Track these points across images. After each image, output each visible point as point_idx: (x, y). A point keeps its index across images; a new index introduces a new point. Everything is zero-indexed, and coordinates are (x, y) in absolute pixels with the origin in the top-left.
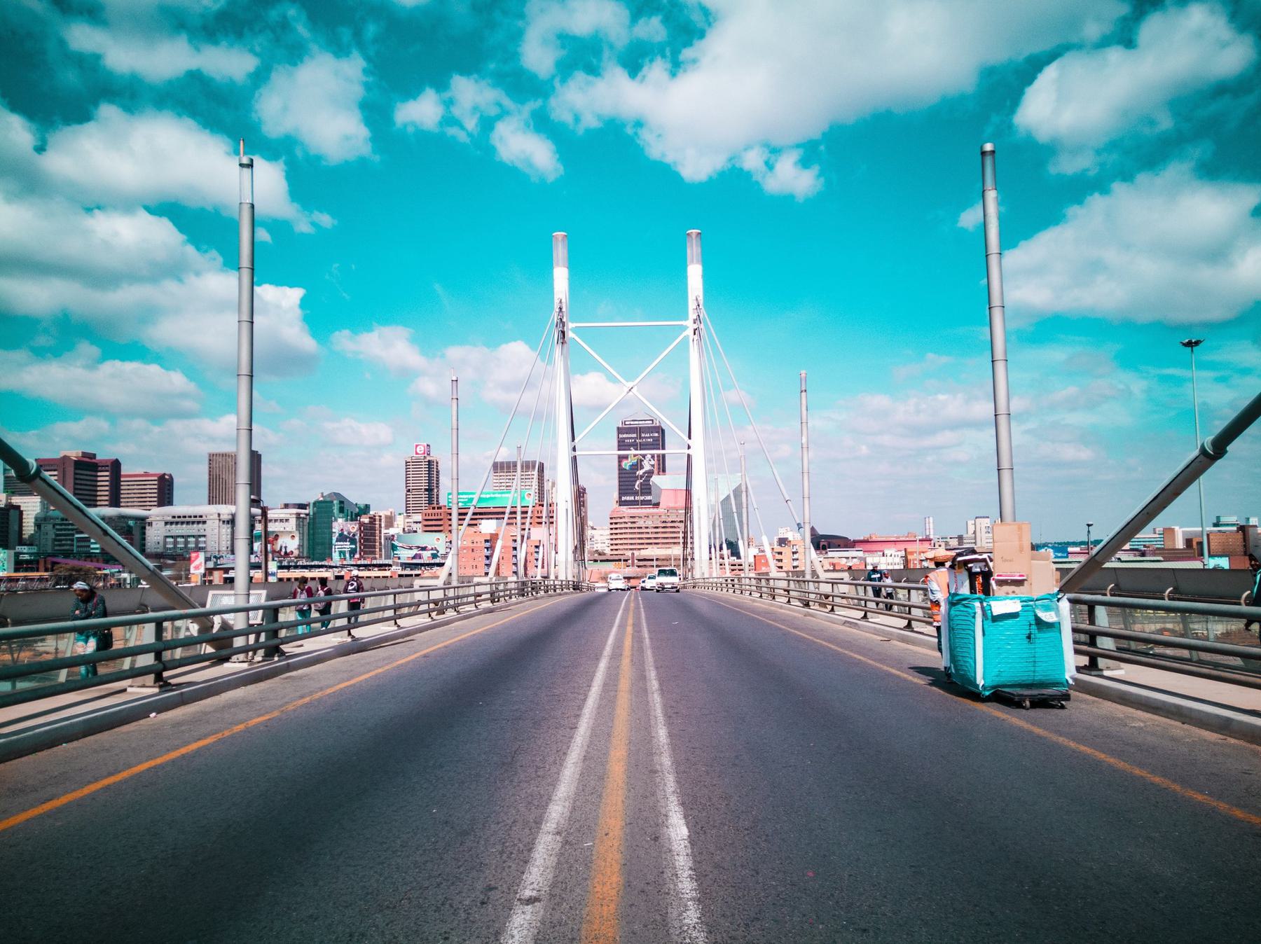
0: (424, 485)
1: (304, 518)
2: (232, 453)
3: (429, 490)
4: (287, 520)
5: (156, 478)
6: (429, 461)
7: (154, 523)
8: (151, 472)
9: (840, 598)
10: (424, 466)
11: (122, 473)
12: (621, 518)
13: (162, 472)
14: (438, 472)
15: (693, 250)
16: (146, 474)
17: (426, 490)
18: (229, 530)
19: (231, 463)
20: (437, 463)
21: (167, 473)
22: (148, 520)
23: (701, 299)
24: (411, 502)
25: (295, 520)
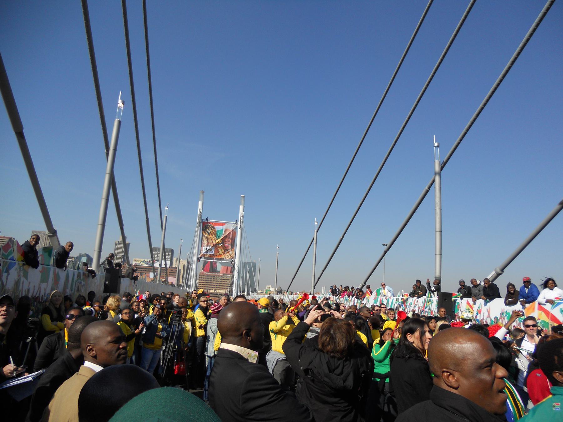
8: (6, 236)
17: (122, 256)
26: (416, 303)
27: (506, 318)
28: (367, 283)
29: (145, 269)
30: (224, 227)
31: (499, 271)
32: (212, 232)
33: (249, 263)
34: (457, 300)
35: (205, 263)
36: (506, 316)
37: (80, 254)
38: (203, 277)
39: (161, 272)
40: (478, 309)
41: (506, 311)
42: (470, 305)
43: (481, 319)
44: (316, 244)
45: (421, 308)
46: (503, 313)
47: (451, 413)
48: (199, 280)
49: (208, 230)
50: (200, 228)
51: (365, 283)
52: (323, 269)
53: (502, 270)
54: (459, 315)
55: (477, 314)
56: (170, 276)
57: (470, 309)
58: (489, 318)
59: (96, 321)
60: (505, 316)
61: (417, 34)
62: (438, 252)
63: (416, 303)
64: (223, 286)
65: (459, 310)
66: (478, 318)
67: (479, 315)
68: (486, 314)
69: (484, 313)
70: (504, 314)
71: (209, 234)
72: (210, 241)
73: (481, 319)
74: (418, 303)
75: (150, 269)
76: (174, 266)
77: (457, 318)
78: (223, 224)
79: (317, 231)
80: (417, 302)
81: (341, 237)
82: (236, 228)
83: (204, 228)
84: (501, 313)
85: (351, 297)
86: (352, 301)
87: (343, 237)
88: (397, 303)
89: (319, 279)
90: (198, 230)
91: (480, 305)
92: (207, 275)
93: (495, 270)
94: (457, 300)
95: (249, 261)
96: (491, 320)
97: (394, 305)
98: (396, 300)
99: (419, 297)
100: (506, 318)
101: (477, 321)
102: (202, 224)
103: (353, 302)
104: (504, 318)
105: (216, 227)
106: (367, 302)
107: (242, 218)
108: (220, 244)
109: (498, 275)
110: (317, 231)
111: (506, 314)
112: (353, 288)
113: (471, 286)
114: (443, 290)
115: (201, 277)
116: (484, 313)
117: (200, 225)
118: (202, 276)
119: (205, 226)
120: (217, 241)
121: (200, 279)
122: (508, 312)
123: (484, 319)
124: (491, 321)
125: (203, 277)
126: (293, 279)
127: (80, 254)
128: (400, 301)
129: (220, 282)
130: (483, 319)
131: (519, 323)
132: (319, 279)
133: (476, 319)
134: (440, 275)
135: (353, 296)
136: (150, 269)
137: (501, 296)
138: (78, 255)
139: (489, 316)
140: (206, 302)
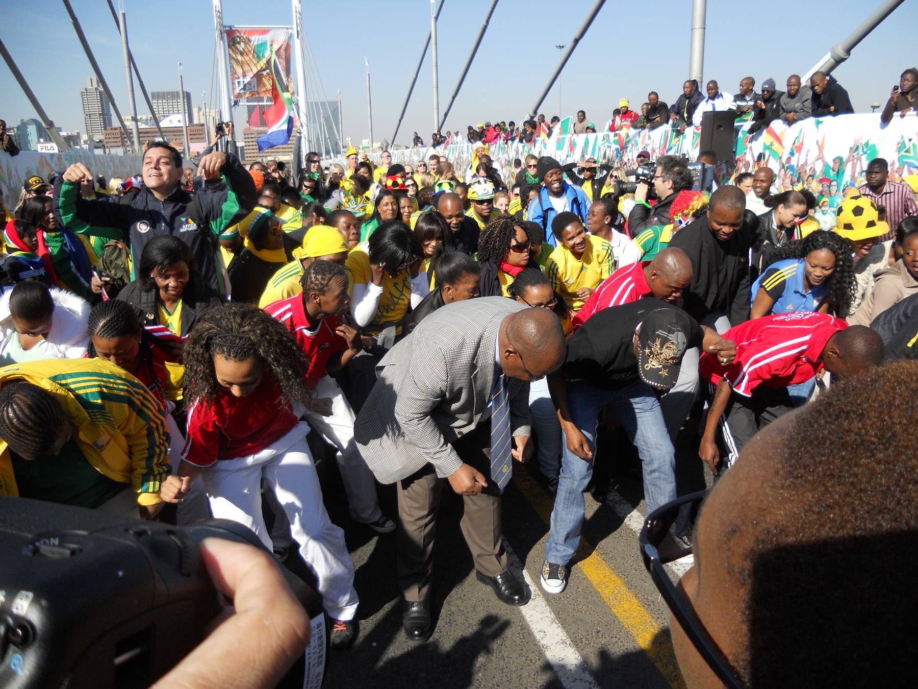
17: (100, 115)
26: (647, 141)
27: (864, 157)
28: (539, 112)
29: (146, 133)
30: (267, 38)
31: (841, 52)
32: (246, 50)
33: (323, 104)
34: (742, 126)
35: (250, 110)
36: (865, 153)
37: (22, 121)
38: (250, 136)
39: (139, 138)
40: (794, 143)
41: (867, 143)
42: (776, 135)
43: (799, 165)
44: (436, 44)
45: (657, 151)
46: (857, 148)
49: (237, 45)
50: (224, 44)
51: (535, 112)
52: (452, 94)
53: (848, 51)
54: (747, 160)
55: (792, 154)
56: (192, 141)
57: (776, 144)
58: (820, 160)
60: (862, 153)
62: (698, 23)
63: (647, 141)
65: (746, 148)
66: (794, 162)
67: (796, 155)
68: (815, 152)
69: (808, 151)
70: (861, 149)
71: (242, 54)
72: (246, 68)
73: (799, 165)
74: (651, 141)
75: (155, 132)
76: (196, 122)
77: (741, 165)
78: (265, 32)
79: (436, 18)
80: (650, 138)
81: (484, 23)
82: (291, 36)
83: (231, 43)
84: (851, 148)
85: (510, 142)
86: (514, 149)
87: (488, 22)
88: (606, 145)
89: (446, 115)
90: (221, 48)
91: (800, 132)
92: (256, 131)
93: (832, 50)
94: (742, 126)
95: (323, 99)
96: (825, 165)
97: (600, 149)
98: (604, 139)
99: (653, 128)
100: (864, 157)
101: (791, 170)
102: (225, 34)
103: (514, 153)
104: (859, 159)
105: (252, 38)
106: (543, 149)
107: (298, 15)
108: (264, 70)
109: (839, 61)
110: (436, 18)
111: (865, 150)
112: (512, 124)
113: (784, 89)
114: (638, 109)
115: (247, 136)
116: (808, 151)
117: (222, 38)
119: (231, 37)
120: (259, 68)
121: (247, 140)
122: (870, 143)
123: (809, 163)
124: (824, 166)
125: (250, 136)
126: (400, 121)
127: (22, 121)
128: (611, 141)
130: (806, 163)
131: (898, 168)
132: (446, 115)
133: (787, 165)
134: (700, 76)
135: (513, 139)
136: (155, 132)
138: (19, 123)
139: (820, 157)
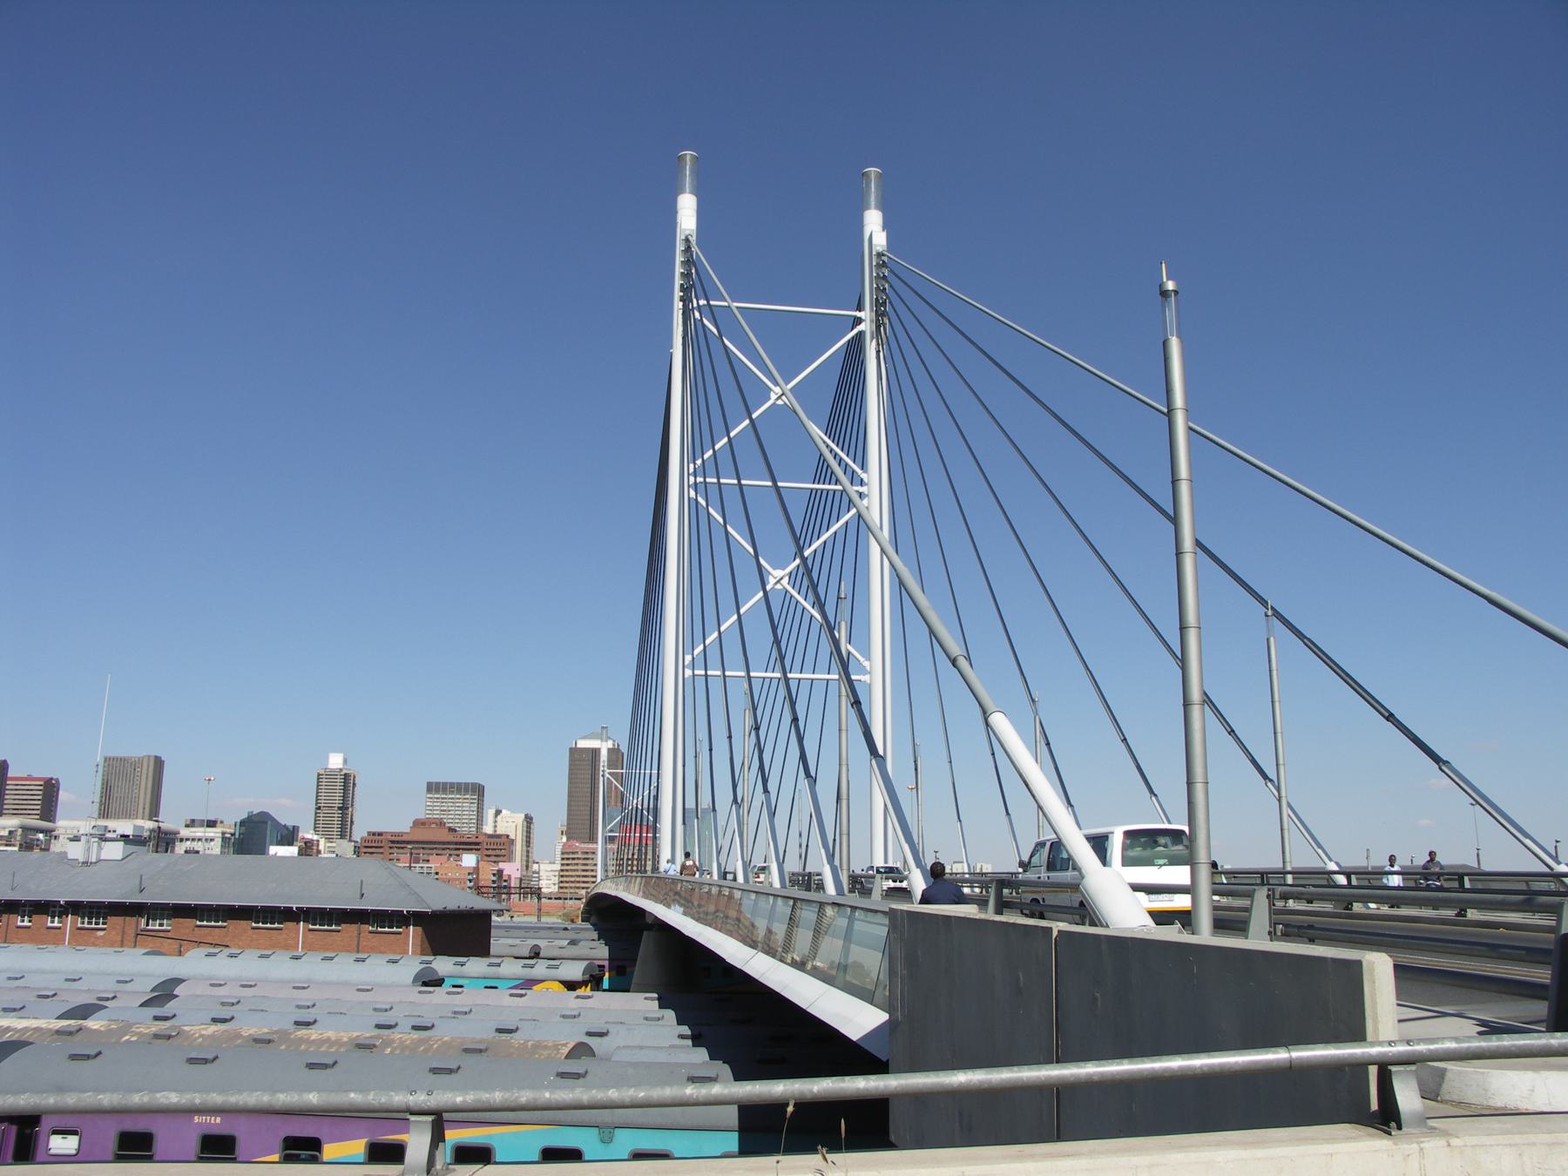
0: (338, 803)
1: (229, 839)
2: (132, 757)
3: (343, 808)
4: (212, 840)
5: (42, 783)
6: (345, 775)
7: (61, 837)
8: (35, 775)
9: (749, 722)
10: (340, 781)
11: (10, 775)
12: (573, 853)
13: (50, 776)
14: (354, 784)
15: (788, 1115)
16: (30, 778)
17: (339, 808)
18: (858, 922)
19: (129, 770)
20: (354, 777)
21: (55, 777)
22: (54, 833)
23: (693, 239)
24: (321, 822)
25: (220, 840)
47: (1332, 867)
48: (562, 865)
59: (102, 1011)
61: (1235, 457)
64: (584, 882)
118: (568, 853)
125: (571, 856)
129: (584, 868)
137: (893, 1138)
140: (791, 902)
